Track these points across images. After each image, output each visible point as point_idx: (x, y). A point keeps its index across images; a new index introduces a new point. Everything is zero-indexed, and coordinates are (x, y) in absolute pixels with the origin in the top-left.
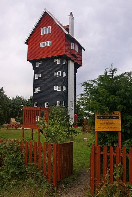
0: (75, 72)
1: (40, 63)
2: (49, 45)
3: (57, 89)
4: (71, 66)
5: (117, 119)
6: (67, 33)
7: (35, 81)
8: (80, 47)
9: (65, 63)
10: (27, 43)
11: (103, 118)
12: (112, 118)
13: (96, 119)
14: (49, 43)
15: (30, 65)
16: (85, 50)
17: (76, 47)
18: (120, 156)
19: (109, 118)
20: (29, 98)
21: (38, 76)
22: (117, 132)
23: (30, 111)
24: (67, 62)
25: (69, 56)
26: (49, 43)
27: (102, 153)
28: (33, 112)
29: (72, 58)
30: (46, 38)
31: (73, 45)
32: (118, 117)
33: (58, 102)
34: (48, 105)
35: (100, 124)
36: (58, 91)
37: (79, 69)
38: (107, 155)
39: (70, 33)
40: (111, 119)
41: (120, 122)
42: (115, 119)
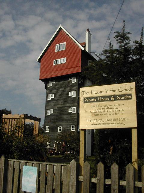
1: (53, 82)
2: (63, 62)
5: (127, 99)
6: (83, 50)
7: (47, 102)
9: (82, 82)
10: (39, 61)
11: (97, 101)
12: (116, 99)
13: (81, 103)
14: (62, 61)
15: (43, 84)
18: (135, 187)
19: (110, 100)
20: (29, 116)
21: (51, 97)
22: (128, 131)
23: (13, 120)
24: (84, 81)
26: (62, 61)
27: (108, 182)
28: (14, 120)
30: (60, 55)
32: (130, 95)
33: (73, 126)
34: (61, 129)
35: (90, 114)
36: (72, 113)
38: (105, 185)
39: (87, 50)
40: (115, 102)
41: (134, 108)
42: (124, 99)
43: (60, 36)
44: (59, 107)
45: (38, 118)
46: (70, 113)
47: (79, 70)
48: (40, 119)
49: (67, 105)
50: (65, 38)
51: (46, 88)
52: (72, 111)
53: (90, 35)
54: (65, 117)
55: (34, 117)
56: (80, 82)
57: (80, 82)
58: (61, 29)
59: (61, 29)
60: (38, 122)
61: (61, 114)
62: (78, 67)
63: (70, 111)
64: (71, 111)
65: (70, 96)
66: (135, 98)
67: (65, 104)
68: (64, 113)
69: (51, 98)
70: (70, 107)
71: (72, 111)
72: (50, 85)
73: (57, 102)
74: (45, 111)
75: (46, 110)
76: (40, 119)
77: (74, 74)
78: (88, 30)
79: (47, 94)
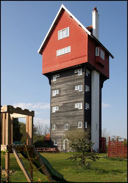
0: (101, 86)
1: (57, 76)
3: (78, 107)
4: (96, 78)
8: (108, 54)
10: (41, 52)
14: (67, 50)
15: (46, 79)
16: (113, 57)
17: (101, 53)
24: (91, 73)
25: (93, 64)
26: (67, 50)
29: (96, 68)
30: (63, 43)
31: (98, 49)
36: (79, 91)
37: (105, 83)
43: (60, 20)
44: (65, 103)
45: (30, 111)
46: (77, 110)
47: (85, 60)
48: (33, 112)
49: (73, 101)
50: (70, 23)
51: (50, 83)
52: (79, 89)
53: (97, 16)
54: (71, 113)
55: (23, 109)
56: (87, 75)
57: (87, 75)
58: (63, 10)
59: (63, 9)
60: (30, 117)
61: (67, 111)
62: (83, 56)
63: (77, 90)
64: (78, 89)
65: (77, 91)
66: (1, 163)
67: (70, 100)
68: (71, 109)
69: (55, 93)
70: (77, 102)
71: (79, 89)
72: (54, 80)
73: (62, 98)
74: (92, 134)
75: (51, 107)
76: (33, 112)
77: (80, 65)
78: (95, 9)
79: (52, 90)
